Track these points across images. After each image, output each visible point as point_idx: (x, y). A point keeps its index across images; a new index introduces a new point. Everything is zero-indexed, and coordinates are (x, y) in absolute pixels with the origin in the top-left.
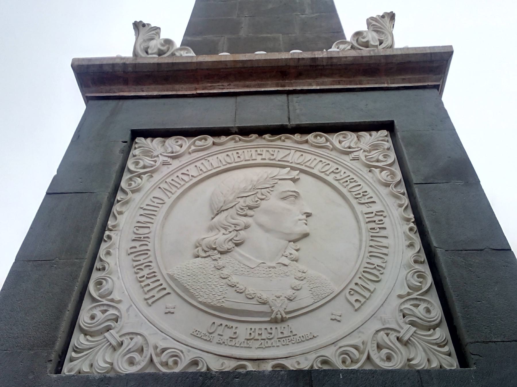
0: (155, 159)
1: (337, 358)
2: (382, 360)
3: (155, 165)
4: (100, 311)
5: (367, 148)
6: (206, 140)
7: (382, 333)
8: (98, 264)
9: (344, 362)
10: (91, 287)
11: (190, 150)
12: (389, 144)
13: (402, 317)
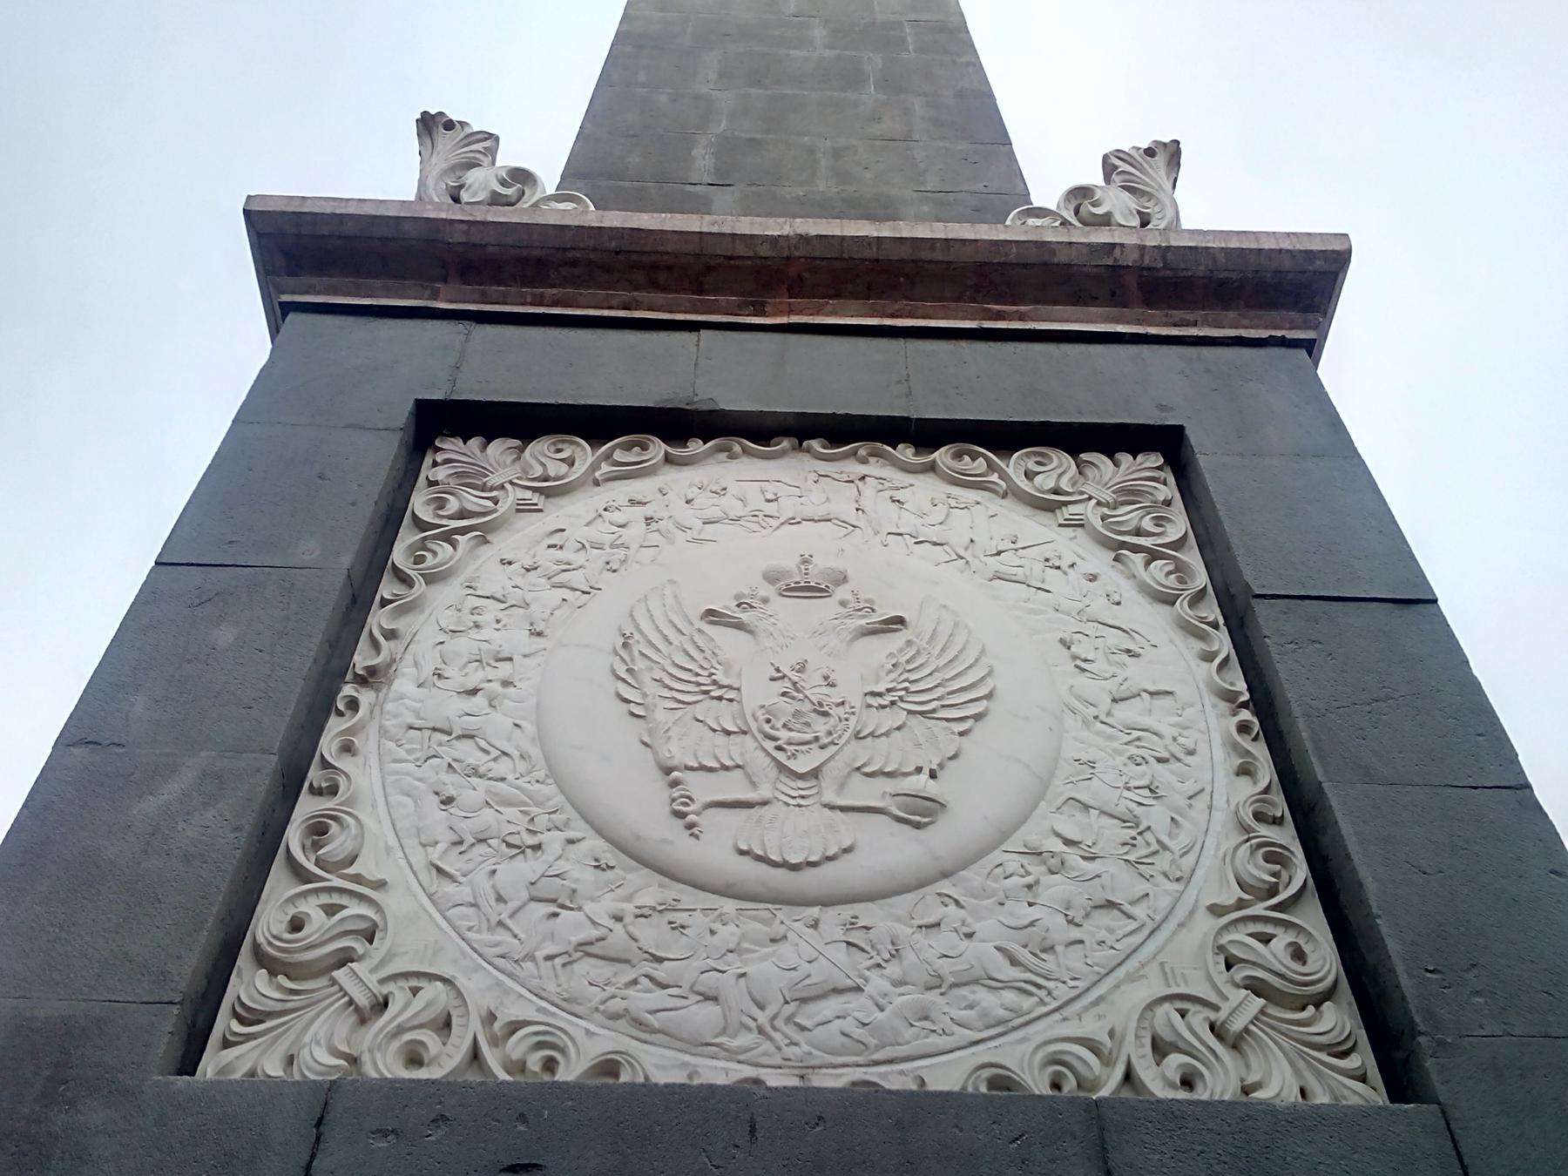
0: (494, 493)
1: (1036, 1071)
2: (1172, 1085)
3: (495, 511)
4: (321, 906)
5: (1108, 496)
7: (1167, 1006)
8: (314, 775)
9: (1056, 1086)
10: (294, 837)
11: (597, 474)
12: (1168, 490)
13: (1223, 966)
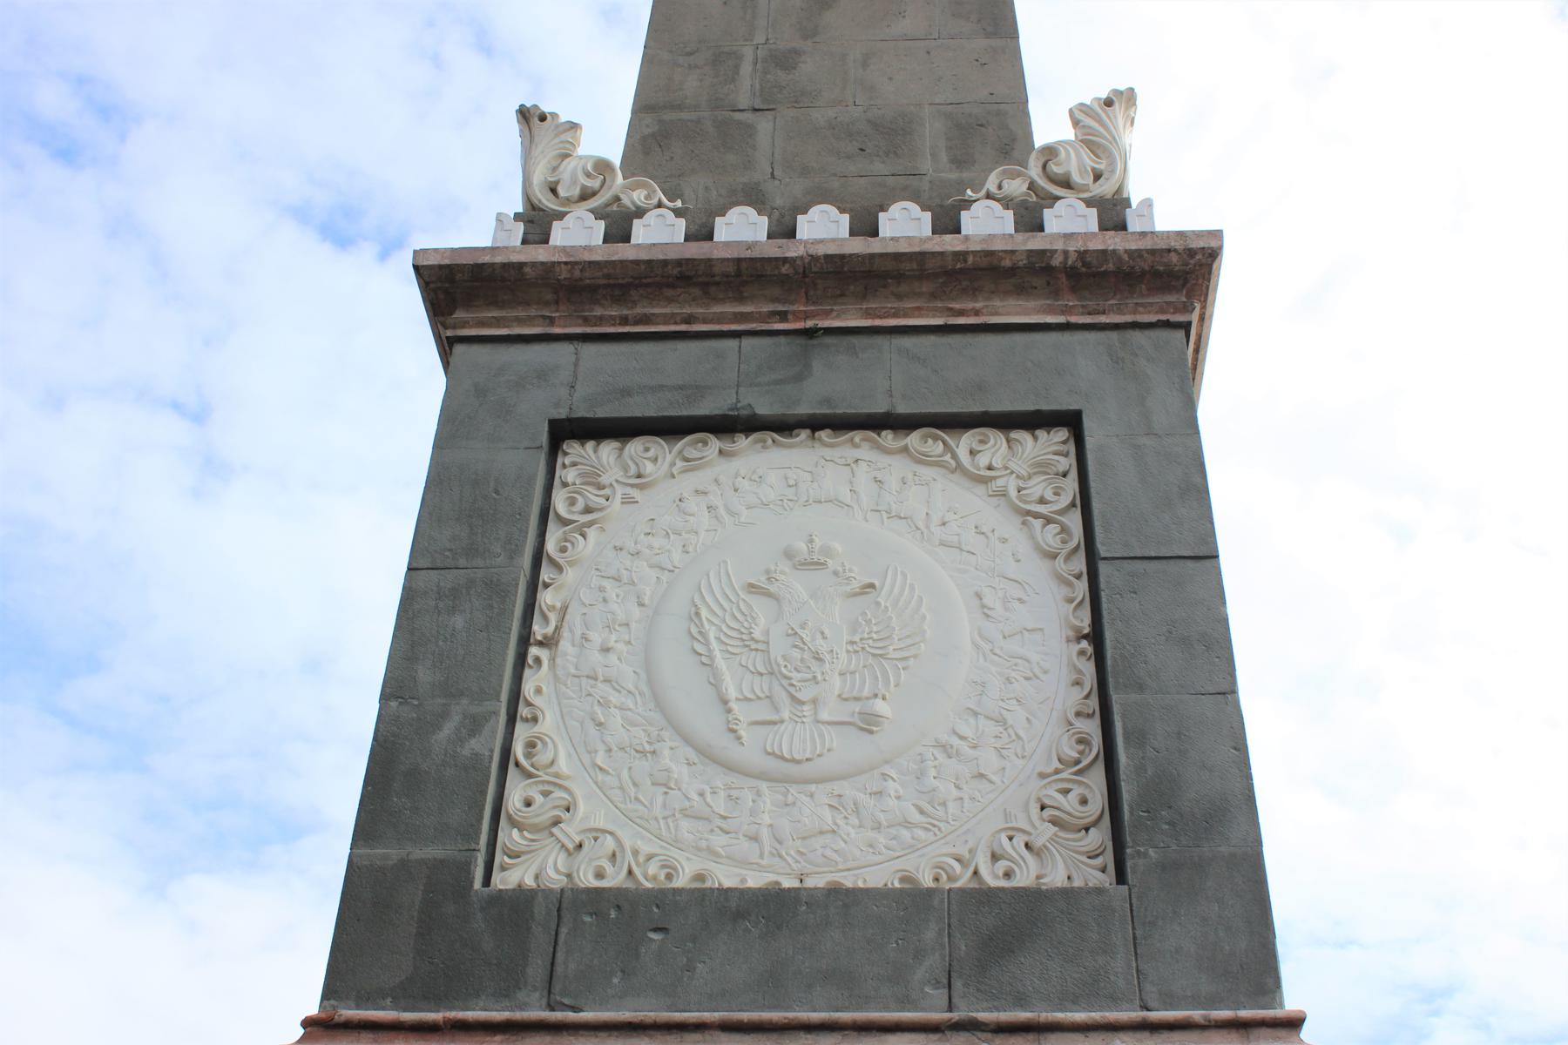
2: (996, 877)
6: (705, 443)
8: (523, 711)
